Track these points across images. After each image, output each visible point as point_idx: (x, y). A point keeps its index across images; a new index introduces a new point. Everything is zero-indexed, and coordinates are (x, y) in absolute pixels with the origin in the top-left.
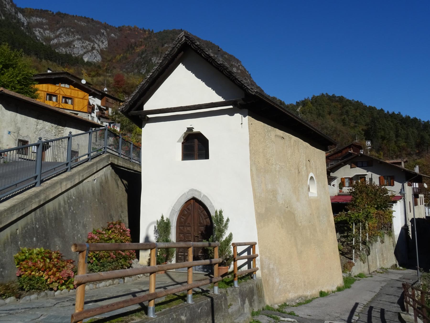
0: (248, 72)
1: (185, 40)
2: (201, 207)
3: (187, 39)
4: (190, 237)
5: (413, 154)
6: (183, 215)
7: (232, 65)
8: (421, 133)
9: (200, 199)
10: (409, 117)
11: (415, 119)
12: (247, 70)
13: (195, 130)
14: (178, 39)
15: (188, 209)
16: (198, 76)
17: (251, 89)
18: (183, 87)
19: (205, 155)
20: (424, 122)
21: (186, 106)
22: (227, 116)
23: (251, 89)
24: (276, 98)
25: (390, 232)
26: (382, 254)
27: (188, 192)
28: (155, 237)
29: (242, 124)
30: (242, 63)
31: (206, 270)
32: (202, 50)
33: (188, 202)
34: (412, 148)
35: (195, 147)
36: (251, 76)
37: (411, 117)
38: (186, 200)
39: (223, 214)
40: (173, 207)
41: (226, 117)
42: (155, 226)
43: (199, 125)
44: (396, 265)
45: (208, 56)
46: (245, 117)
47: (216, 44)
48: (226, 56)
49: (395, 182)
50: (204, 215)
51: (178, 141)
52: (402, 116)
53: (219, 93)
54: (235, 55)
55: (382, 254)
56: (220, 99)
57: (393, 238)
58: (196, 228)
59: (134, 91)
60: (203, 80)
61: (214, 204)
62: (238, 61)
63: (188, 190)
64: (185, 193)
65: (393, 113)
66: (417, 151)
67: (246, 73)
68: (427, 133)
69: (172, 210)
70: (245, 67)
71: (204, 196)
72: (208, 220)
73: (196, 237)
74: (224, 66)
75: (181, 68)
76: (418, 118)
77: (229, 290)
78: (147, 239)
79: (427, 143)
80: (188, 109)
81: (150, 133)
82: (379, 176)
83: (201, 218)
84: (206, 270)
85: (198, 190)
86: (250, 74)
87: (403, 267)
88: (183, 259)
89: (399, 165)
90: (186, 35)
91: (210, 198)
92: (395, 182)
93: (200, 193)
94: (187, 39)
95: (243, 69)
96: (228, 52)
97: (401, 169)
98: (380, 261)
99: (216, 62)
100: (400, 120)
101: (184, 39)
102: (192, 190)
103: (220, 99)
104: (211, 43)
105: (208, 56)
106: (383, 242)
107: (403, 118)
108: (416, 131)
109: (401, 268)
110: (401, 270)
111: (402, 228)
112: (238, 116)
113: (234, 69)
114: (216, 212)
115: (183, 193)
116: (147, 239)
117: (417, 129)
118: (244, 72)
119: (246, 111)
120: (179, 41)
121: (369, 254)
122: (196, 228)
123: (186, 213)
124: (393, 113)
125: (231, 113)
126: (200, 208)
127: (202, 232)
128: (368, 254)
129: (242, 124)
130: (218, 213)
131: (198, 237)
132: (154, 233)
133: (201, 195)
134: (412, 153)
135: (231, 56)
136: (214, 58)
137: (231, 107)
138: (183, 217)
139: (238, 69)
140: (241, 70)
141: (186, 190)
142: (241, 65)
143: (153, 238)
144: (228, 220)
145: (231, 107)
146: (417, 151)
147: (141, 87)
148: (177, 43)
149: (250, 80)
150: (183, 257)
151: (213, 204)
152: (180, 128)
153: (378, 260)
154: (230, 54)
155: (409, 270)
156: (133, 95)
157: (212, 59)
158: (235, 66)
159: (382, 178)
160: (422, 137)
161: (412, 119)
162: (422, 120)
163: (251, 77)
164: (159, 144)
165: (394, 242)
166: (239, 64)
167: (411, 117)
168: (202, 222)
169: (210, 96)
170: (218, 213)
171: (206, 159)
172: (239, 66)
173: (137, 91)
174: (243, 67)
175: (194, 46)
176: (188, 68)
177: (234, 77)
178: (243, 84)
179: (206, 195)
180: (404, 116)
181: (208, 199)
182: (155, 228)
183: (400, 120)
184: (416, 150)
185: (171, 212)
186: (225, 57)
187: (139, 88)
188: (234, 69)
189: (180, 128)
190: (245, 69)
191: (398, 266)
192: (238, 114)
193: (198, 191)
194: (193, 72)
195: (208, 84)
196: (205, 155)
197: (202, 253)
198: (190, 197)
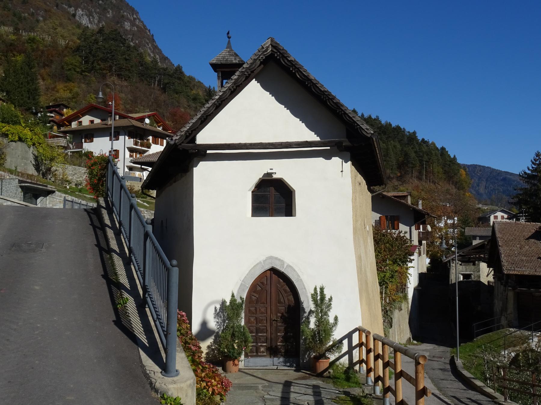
0: (149, 31)
1: (272, 50)
2: (281, 281)
3: (275, 50)
4: (265, 322)
5: (392, 178)
6: (254, 292)
7: (123, 16)
8: (405, 149)
9: (282, 270)
10: (390, 125)
11: (398, 128)
14: (263, 48)
15: (262, 283)
16: (280, 100)
18: (255, 114)
20: (409, 132)
21: (269, 143)
22: (321, 159)
24: (194, 79)
25: (405, 297)
26: (400, 326)
27: (264, 261)
28: (216, 323)
29: (342, 171)
30: (142, 16)
31: (288, 364)
32: (298, 68)
33: (263, 275)
34: (392, 169)
35: (273, 198)
39: (325, 292)
40: (243, 281)
41: (320, 161)
42: (216, 308)
45: (306, 78)
46: (346, 162)
50: (285, 291)
52: (380, 122)
53: (310, 127)
55: (400, 326)
57: (408, 303)
58: (273, 308)
60: (287, 107)
62: (133, 11)
63: (264, 258)
64: (260, 262)
67: (146, 33)
68: (412, 148)
70: (145, 24)
71: (289, 266)
72: (291, 298)
73: (274, 320)
75: (254, 86)
76: (402, 127)
77: (367, 389)
79: (412, 164)
80: (271, 147)
81: (203, 173)
83: (281, 295)
84: (288, 364)
85: (279, 258)
86: (153, 36)
87: (417, 341)
90: (274, 45)
91: (297, 270)
93: (282, 262)
94: (275, 50)
95: (141, 25)
97: (406, 206)
100: (378, 128)
101: (270, 49)
102: (271, 258)
105: (306, 78)
106: (401, 310)
107: (382, 126)
108: (398, 146)
109: (415, 342)
110: (414, 344)
111: (414, 289)
112: (336, 161)
113: (126, 23)
114: (315, 289)
115: (258, 262)
116: (204, 324)
117: (399, 142)
118: (143, 32)
119: (348, 154)
122: (273, 308)
123: (259, 288)
124: (370, 117)
125: (327, 156)
128: (390, 326)
129: (342, 171)
130: (318, 290)
131: (276, 321)
132: (215, 318)
133: (284, 264)
134: (392, 176)
137: (329, 148)
138: (255, 294)
139: (133, 24)
140: (137, 27)
142: (139, 19)
143: (213, 324)
144: (330, 299)
145: (329, 148)
146: (399, 174)
147: (205, 111)
149: (153, 45)
150: (255, 348)
151: (302, 277)
152: (255, 170)
156: (194, 121)
158: (129, 20)
159: (384, 218)
160: (406, 155)
163: (153, 41)
165: (408, 308)
166: (135, 16)
168: (282, 300)
169: (299, 131)
172: (135, 19)
173: (199, 116)
174: (142, 22)
175: (286, 61)
176: (265, 87)
177: (342, 110)
178: (355, 122)
179: (291, 264)
180: (383, 122)
181: (295, 270)
182: (216, 310)
183: (378, 128)
184: (397, 172)
185: (239, 288)
187: (202, 113)
188: (126, 23)
189: (255, 170)
190: (145, 26)
191: (412, 340)
192: (337, 158)
193: (279, 260)
195: (295, 113)
197: (282, 342)
198: (268, 267)
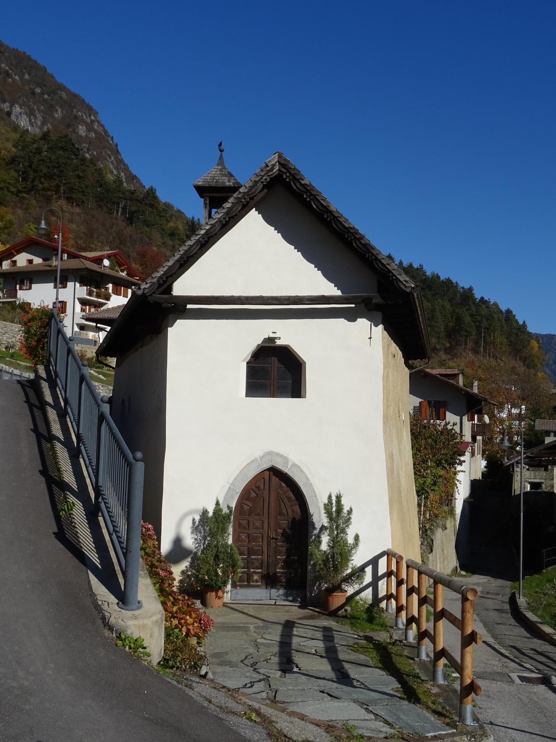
0: (112, 138)
1: (279, 170)
2: (284, 485)
3: (283, 170)
4: (260, 540)
7: (76, 117)
9: (285, 470)
10: (438, 277)
11: (449, 281)
12: (111, 134)
13: (278, 342)
14: (267, 166)
15: (258, 488)
17: (405, 281)
18: (254, 257)
19: (296, 390)
20: (463, 288)
23: (405, 281)
24: (172, 207)
27: (261, 458)
28: (193, 540)
29: (370, 338)
31: (291, 598)
32: (314, 196)
35: (276, 372)
36: (119, 148)
37: (442, 278)
38: (259, 470)
39: (343, 501)
40: (232, 484)
42: (194, 520)
43: (290, 333)
44: (457, 567)
45: (324, 209)
46: (376, 326)
47: (41, 62)
48: (64, 95)
49: (447, 412)
50: (289, 499)
51: (243, 361)
52: (424, 273)
54: (83, 95)
55: (443, 550)
56: (336, 292)
58: (272, 523)
59: (171, 257)
61: (312, 481)
62: (90, 110)
63: (261, 453)
64: (256, 460)
65: (411, 265)
66: (448, 345)
69: (229, 489)
71: (295, 465)
72: (297, 508)
73: (273, 538)
74: (356, 233)
77: (396, 633)
78: (178, 541)
79: (466, 331)
80: (274, 302)
81: (183, 338)
82: (420, 400)
83: (283, 505)
84: (291, 598)
85: (282, 453)
86: (117, 145)
87: (466, 571)
88: (246, 579)
89: (453, 379)
90: (283, 162)
91: (305, 470)
92: (447, 412)
94: (283, 170)
95: (100, 129)
96: (68, 87)
97: (457, 388)
98: (440, 563)
99: (340, 222)
100: (421, 281)
101: (277, 168)
102: (270, 453)
103: (336, 292)
104: (29, 58)
105: (324, 209)
106: (446, 528)
107: (427, 278)
108: (448, 307)
109: (463, 573)
112: (363, 323)
113: (80, 127)
114: (330, 497)
115: (253, 458)
116: (178, 541)
118: (103, 140)
119: (379, 315)
120: (269, 171)
121: (432, 551)
123: (253, 495)
124: (411, 265)
125: (351, 316)
126: (281, 486)
127: (284, 530)
128: (429, 550)
129: (370, 338)
130: (334, 499)
131: (276, 539)
132: (192, 533)
133: (287, 463)
134: (438, 347)
135: (75, 96)
136: (336, 215)
138: (247, 503)
139: (90, 128)
140: (96, 132)
141: (258, 454)
142: (99, 122)
144: (350, 512)
145: (353, 306)
146: (448, 345)
147: (186, 251)
148: (263, 174)
149: (116, 158)
150: (246, 575)
153: (438, 561)
154: (73, 90)
155: (477, 576)
156: (170, 264)
157: (334, 216)
160: (459, 319)
161: (443, 282)
162: (461, 285)
164: (201, 363)
166: (93, 118)
167: (442, 278)
169: (313, 282)
170: (334, 499)
171: (293, 396)
172: (92, 121)
173: (177, 257)
174: (102, 126)
175: (298, 185)
176: (269, 220)
178: (389, 271)
179: (297, 463)
180: (428, 273)
181: (302, 471)
183: (421, 281)
185: (227, 494)
186: (60, 97)
188: (80, 127)
190: (106, 132)
192: (365, 319)
193: (282, 456)
194: (278, 229)
196: (296, 390)
197: (282, 568)
